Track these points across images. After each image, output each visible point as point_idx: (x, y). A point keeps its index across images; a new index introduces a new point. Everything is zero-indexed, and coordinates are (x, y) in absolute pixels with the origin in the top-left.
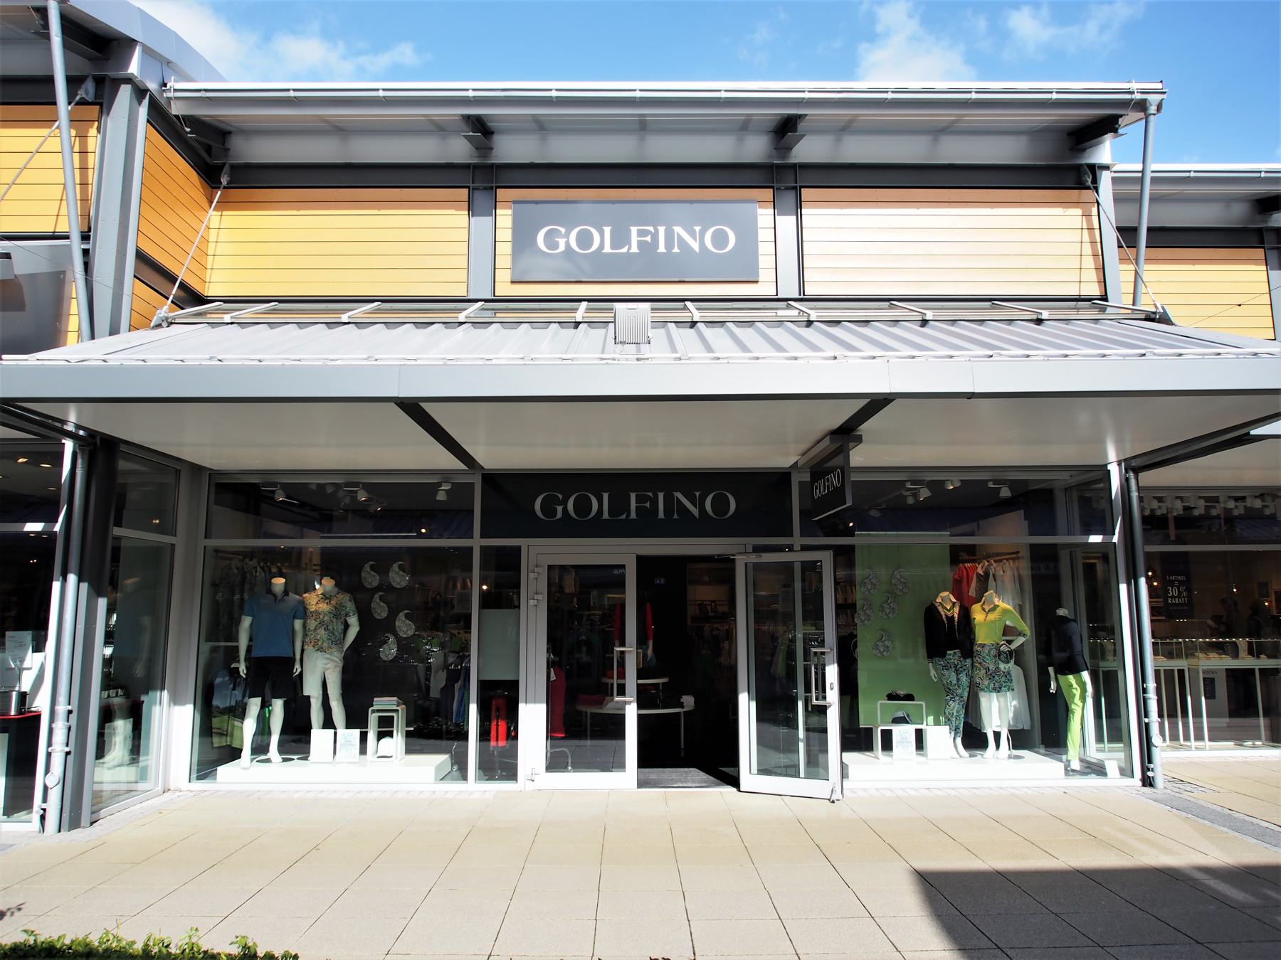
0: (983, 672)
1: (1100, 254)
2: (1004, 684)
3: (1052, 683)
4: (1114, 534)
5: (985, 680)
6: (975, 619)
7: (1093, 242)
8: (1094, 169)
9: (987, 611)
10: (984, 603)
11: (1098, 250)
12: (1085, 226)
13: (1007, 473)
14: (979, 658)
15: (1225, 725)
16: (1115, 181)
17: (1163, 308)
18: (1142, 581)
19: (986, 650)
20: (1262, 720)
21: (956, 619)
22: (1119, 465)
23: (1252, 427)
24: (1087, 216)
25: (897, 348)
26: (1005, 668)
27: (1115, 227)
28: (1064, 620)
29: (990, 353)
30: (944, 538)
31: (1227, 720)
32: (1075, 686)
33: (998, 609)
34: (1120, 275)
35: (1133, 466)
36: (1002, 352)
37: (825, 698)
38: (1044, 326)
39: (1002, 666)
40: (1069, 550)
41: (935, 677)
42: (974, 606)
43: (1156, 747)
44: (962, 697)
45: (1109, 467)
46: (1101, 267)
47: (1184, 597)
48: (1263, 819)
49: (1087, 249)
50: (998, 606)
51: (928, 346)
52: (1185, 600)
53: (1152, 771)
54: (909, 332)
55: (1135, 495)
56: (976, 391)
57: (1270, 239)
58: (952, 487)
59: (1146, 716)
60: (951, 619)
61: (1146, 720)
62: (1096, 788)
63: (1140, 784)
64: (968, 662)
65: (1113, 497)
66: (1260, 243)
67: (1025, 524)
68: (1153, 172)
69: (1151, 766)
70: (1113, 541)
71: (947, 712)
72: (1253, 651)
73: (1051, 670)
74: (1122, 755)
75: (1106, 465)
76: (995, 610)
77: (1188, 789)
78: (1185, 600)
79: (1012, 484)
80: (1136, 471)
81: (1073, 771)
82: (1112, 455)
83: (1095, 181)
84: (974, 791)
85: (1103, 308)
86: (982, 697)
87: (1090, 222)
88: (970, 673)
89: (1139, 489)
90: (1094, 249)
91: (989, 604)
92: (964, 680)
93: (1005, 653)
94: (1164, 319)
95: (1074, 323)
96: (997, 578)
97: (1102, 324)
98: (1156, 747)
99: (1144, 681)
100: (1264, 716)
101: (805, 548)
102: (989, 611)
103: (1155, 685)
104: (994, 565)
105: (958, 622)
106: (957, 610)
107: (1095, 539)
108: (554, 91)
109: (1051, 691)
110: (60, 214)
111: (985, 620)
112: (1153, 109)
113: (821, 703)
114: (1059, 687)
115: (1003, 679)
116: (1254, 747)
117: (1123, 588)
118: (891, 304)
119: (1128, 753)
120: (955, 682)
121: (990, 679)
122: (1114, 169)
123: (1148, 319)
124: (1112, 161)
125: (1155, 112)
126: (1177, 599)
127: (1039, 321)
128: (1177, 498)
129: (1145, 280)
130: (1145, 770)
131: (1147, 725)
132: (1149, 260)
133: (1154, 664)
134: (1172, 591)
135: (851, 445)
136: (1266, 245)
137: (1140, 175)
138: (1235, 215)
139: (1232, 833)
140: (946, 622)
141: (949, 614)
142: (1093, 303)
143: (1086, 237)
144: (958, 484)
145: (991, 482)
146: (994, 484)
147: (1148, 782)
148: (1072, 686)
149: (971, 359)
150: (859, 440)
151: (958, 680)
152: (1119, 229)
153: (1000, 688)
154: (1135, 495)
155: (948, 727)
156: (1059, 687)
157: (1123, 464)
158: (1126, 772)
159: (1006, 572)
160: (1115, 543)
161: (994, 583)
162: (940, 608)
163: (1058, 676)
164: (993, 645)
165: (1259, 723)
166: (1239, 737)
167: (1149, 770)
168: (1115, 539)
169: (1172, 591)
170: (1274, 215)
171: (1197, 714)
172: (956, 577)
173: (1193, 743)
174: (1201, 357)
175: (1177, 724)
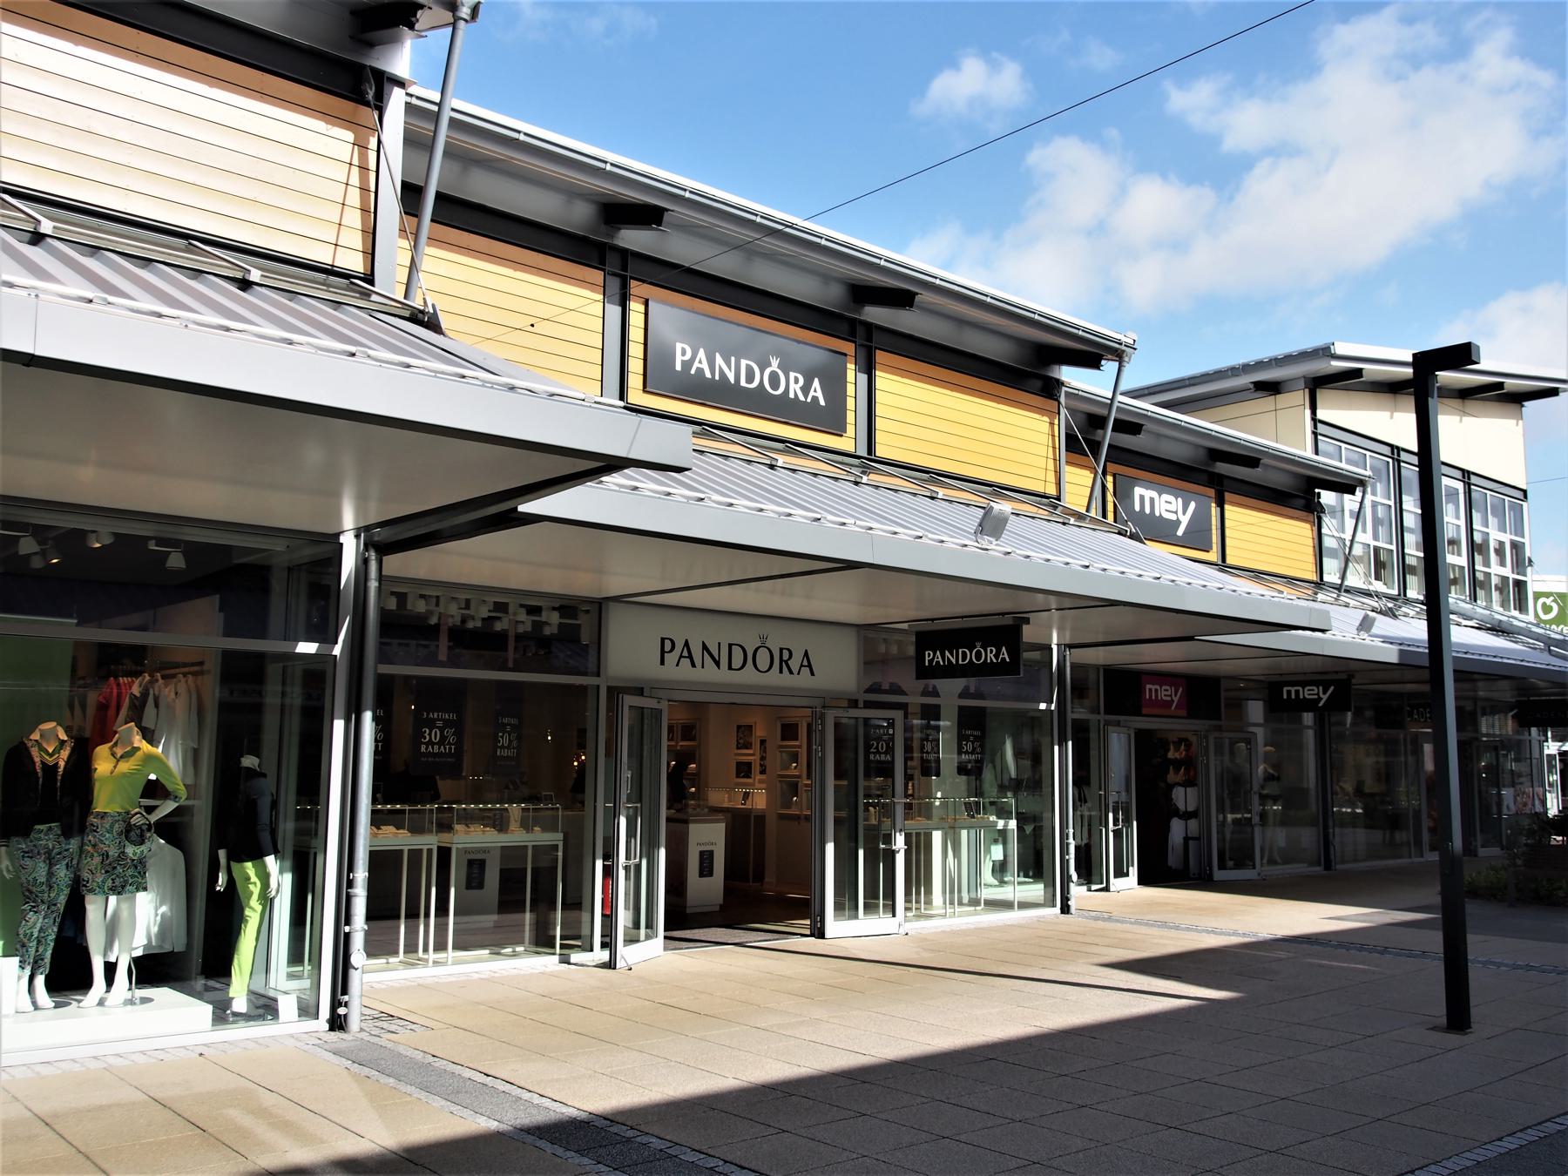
0: (97, 859)
1: (372, 210)
2: (44, 886)
3: (220, 874)
5: (98, 875)
6: (96, 769)
7: (364, 189)
8: (385, 82)
9: (119, 756)
10: (116, 744)
11: (370, 204)
12: (356, 161)
13: (186, 530)
14: (95, 837)
15: (492, 924)
16: (410, 109)
17: (433, 306)
18: (368, 716)
19: (107, 823)
20: (528, 915)
21: (61, 770)
22: (357, 536)
23: (519, 499)
26: (135, 854)
28: (252, 773)
30: (64, 629)
31: (495, 917)
32: (254, 878)
33: (139, 754)
34: (394, 252)
35: (1066, 647)
39: (130, 850)
40: (281, 665)
41: (8, 871)
42: (99, 748)
43: (356, 969)
44: (55, 905)
45: (342, 539)
46: (371, 231)
47: (449, 743)
48: (471, 1065)
49: (354, 197)
50: (138, 749)
52: (450, 749)
53: (346, 1005)
55: (373, 584)
56: (37, 353)
57: (613, 261)
58: (98, 545)
59: (348, 922)
60: (50, 770)
61: (347, 929)
62: (255, 1041)
63: (327, 1027)
64: (74, 844)
65: (342, 587)
66: (599, 264)
67: (219, 619)
68: (453, 110)
69: (346, 998)
70: (334, 653)
71: (21, 932)
72: (526, 826)
73: (222, 854)
74: (306, 983)
75: (338, 535)
76: (132, 755)
77: (393, 1028)
78: (450, 749)
79: (192, 551)
80: (384, 549)
81: (235, 1014)
82: (349, 520)
84: (39, 1068)
86: (89, 903)
87: (363, 157)
88: (75, 862)
89: (381, 578)
90: (364, 200)
91: (124, 746)
92: (62, 875)
93: (140, 827)
94: (432, 324)
96: (162, 704)
98: (356, 969)
99: (351, 869)
100: (531, 911)
102: (122, 757)
103: (367, 874)
104: (161, 681)
105: (63, 776)
106: (65, 754)
107: (307, 648)
109: (218, 888)
111: (112, 773)
114: (231, 882)
115: (130, 872)
116: (515, 955)
117: (339, 726)
119: (316, 977)
120: (43, 880)
121: (107, 872)
122: (411, 90)
125: (468, 18)
126: (436, 747)
127: (245, 285)
128: (422, 596)
130: (335, 1004)
131: (347, 936)
132: (434, 241)
133: (371, 841)
134: (430, 734)
136: (607, 268)
138: (577, 217)
139: (423, 1095)
140: (40, 774)
141: (50, 761)
142: (352, 283)
143: (355, 179)
144: (108, 540)
145: (154, 541)
146: (157, 546)
147: (337, 1023)
148: (249, 879)
151: (50, 874)
153: (123, 887)
154: (373, 584)
155: (16, 960)
156: (231, 882)
157: (362, 535)
158: (307, 1010)
159: (175, 696)
160: (336, 656)
161: (155, 710)
162: (35, 752)
163: (232, 863)
164: (119, 814)
165: (524, 920)
166: (496, 941)
167: (340, 1005)
168: (337, 650)
169: (430, 734)
170: (623, 231)
171: (442, 910)
172: (101, 699)
173: (432, 956)
174: (433, 374)
175: (399, 927)
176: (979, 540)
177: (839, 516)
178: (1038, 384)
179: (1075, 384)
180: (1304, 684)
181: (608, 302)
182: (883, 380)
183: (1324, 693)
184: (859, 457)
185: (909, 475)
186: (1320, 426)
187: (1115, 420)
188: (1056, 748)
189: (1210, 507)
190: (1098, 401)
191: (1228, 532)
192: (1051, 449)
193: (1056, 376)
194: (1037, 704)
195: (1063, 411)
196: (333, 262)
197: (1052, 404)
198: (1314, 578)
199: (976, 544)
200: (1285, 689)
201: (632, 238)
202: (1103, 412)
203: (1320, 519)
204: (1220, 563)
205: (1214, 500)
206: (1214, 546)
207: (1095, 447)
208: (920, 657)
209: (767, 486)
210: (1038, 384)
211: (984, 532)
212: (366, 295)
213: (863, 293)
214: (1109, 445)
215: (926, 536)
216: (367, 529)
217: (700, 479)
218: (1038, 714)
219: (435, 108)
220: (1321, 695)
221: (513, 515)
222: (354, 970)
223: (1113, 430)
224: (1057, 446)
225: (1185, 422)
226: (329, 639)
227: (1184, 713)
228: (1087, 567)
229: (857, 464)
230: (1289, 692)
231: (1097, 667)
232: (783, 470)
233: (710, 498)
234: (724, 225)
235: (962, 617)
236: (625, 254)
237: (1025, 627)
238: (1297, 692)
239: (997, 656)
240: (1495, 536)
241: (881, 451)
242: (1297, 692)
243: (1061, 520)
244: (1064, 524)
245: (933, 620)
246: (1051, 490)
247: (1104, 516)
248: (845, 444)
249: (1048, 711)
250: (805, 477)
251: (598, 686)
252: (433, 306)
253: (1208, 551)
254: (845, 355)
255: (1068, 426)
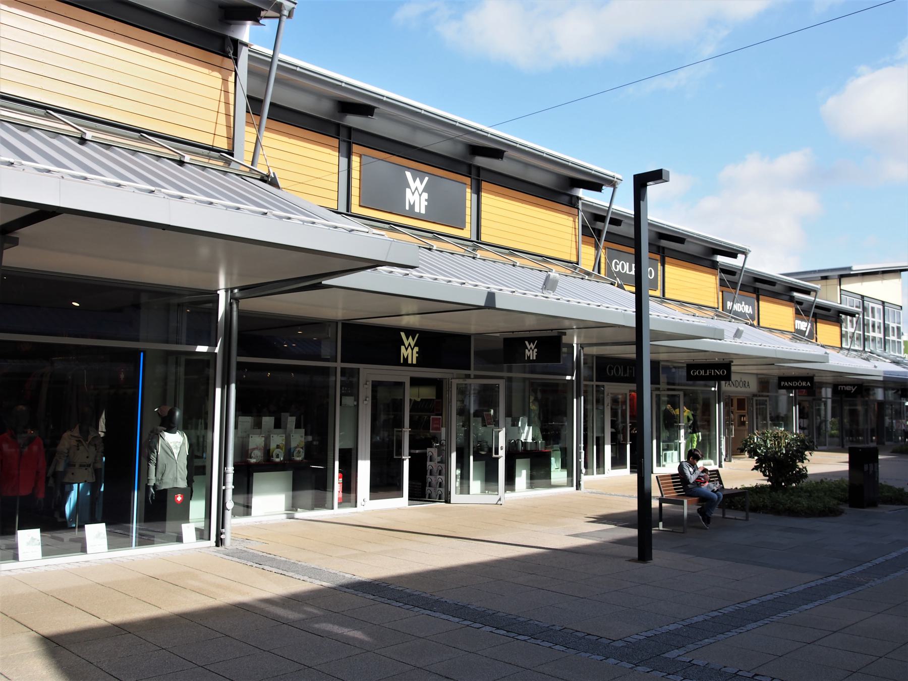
4: (217, 346)
17: (274, 173)
23: (324, 279)
24: (225, 80)
25: (70, 167)
27: (246, 95)
29: (153, 188)
32: (696, 437)
35: (581, 346)
36: (163, 190)
37: (498, 454)
38: (136, 157)
43: (229, 510)
45: (574, 345)
51: (135, 180)
54: (71, 148)
55: (582, 358)
59: (224, 485)
61: (224, 488)
63: (215, 544)
65: (219, 320)
66: (337, 135)
68: (279, 61)
69: (223, 530)
82: (222, 284)
83: (236, 54)
85: (228, 161)
90: (228, 121)
94: (274, 183)
95: (209, 171)
97: (229, 177)
98: (229, 510)
99: (225, 465)
101: (477, 377)
108: (457, 123)
110: (216, 136)
112: (286, 13)
113: (497, 456)
117: (218, 391)
118: (47, 112)
123: (263, 180)
124: (250, 41)
127: (181, 163)
129: (262, 144)
130: (219, 534)
131: (224, 491)
135: (6, 245)
137: (270, 60)
138: (322, 108)
143: (222, 109)
149: (197, 203)
150: (15, 242)
152: (249, 97)
154: (582, 358)
168: (217, 350)
176: (544, 292)
177: (499, 286)
178: (567, 198)
179: (586, 198)
180: (846, 385)
181: (341, 156)
182: (485, 196)
183: (854, 388)
184: (472, 241)
185: (499, 251)
186: (842, 291)
187: (611, 218)
188: (575, 400)
189: (465, 192)
190: (589, 205)
191: (483, 215)
192: (574, 236)
193: (715, 259)
194: (564, 377)
195: (581, 214)
196: (213, 143)
197: (575, 211)
198: (840, 346)
199: (542, 295)
200: (839, 387)
201: (354, 121)
202: (604, 214)
203: (841, 325)
204: (662, 297)
205: (659, 261)
206: (468, 225)
207: (599, 233)
208: (780, 384)
209: (435, 264)
210: (708, 263)
211: (547, 288)
212: (228, 162)
213: (476, 150)
214: (607, 232)
215: (517, 291)
216: (232, 289)
217: (426, 269)
218: (566, 382)
219: (270, 60)
220: (852, 389)
221: (319, 285)
222: (227, 511)
223: (609, 223)
224: (577, 234)
225: (425, 111)
226: (572, 375)
227: (806, 394)
228: (599, 306)
229: (471, 245)
230: (841, 388)
231: (593, 356)
232: (436, 251)
233: (411, 274)
234: (424, 122)
235: (529, 331)
236: (350, 129)
237: (563, 337)
238: (844, 388)
239: (806, 384)
240: (892, 325)
241: (484, 238)
242: (844, 388)
243: (581, 277)
244: (582, 279)
245: (513, 332)
246: (574, 259)
247: (599, 272)
248: (466, 233)
249: (572, 380)
250: (447, 255)
251: (336, 368)
252: (274, 173)
253: (463, 229)
254: (466, 184)
255: (583, 221)
